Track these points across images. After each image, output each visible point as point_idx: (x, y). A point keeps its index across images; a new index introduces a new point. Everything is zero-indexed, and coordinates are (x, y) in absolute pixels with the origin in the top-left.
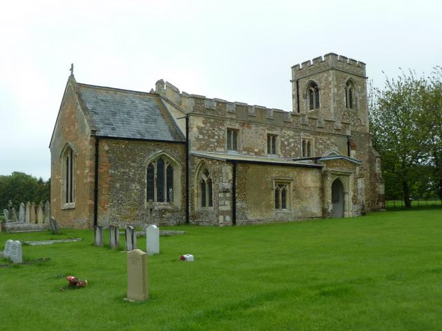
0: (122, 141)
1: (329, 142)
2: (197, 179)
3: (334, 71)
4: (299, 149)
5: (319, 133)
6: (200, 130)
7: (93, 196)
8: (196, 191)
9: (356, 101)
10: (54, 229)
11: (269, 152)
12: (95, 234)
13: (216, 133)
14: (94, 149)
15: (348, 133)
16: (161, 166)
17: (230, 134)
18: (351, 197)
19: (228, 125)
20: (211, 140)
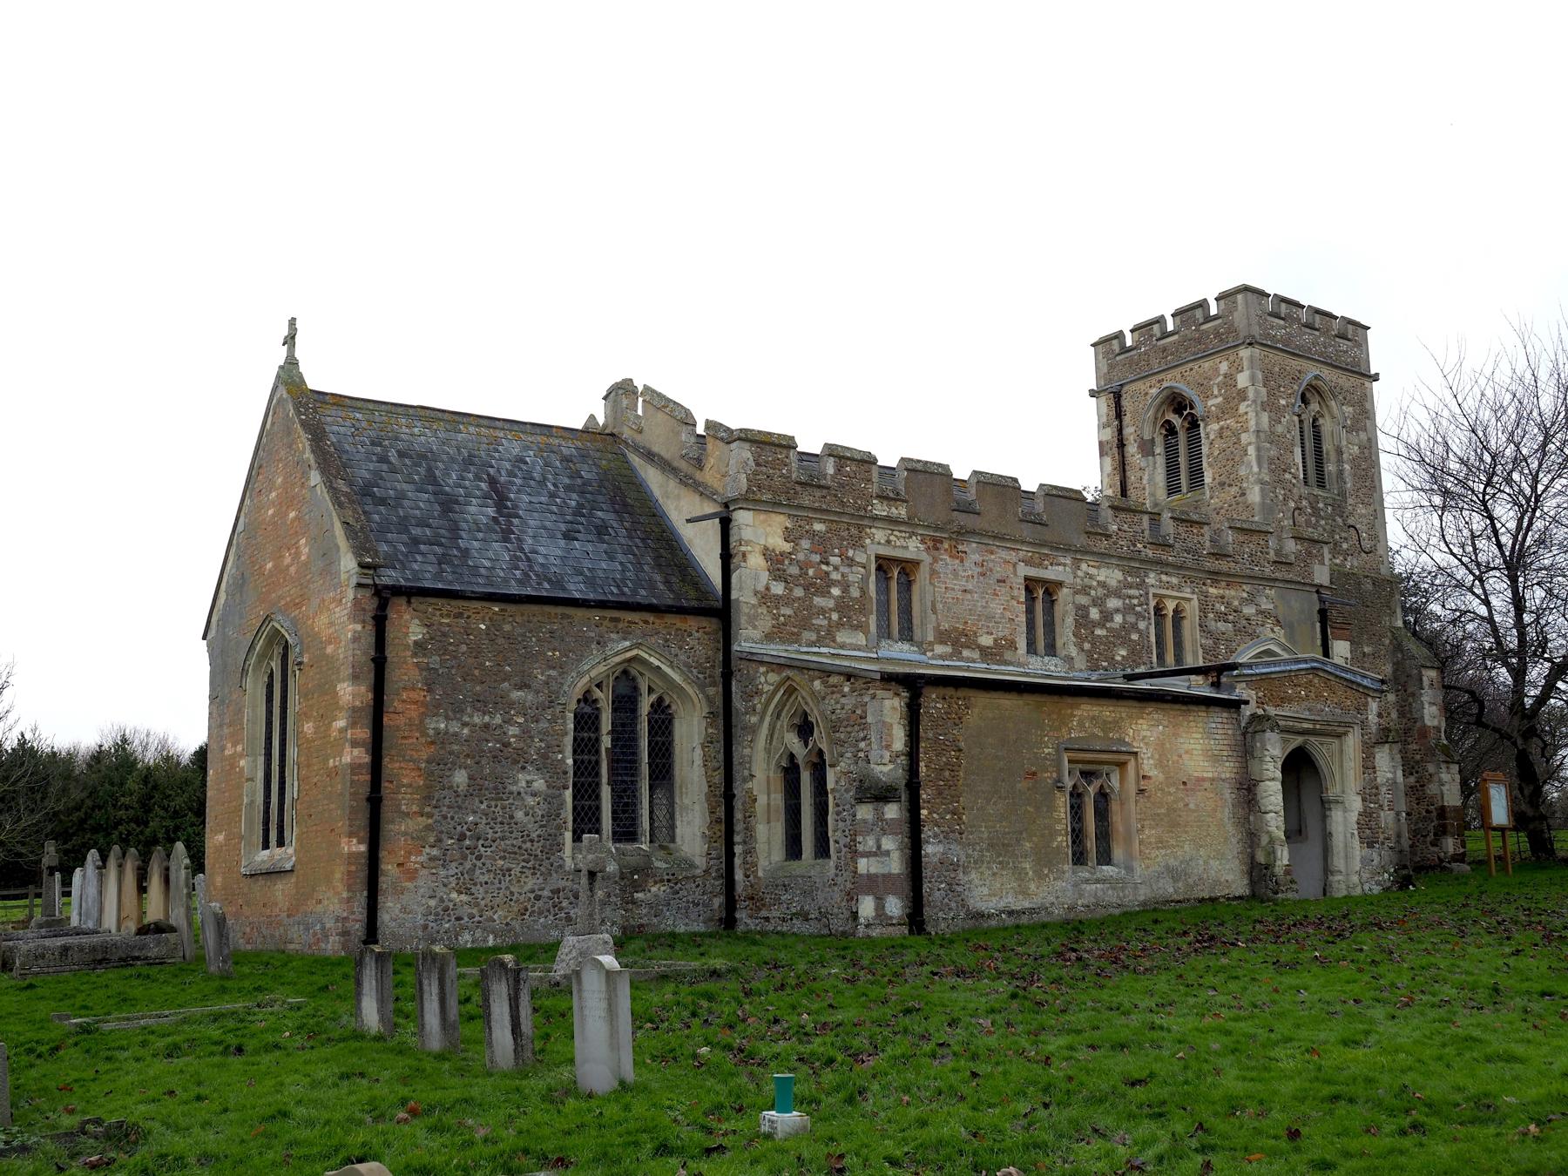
0: (478, 605)
1: (1249, 610)
2: (768, 751)
3: (1257, 351)
4: (1144, 635)
5: (1215, 577)
6: (775, 561)
7: (363, 820)
8: (762, 800)
9: (1340, 461)
10: (1505, 620)
11: (1032, 648)
12: (359, 983)
13: (835, 576)
14: (369, 639)
15: (1321, 575)
16: (625, 704)
17: (888, 579)
18: (1354, 817)
19: (879, 541)
20: (818, 601)
